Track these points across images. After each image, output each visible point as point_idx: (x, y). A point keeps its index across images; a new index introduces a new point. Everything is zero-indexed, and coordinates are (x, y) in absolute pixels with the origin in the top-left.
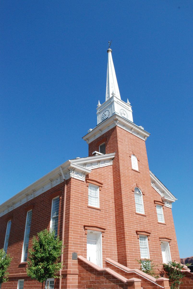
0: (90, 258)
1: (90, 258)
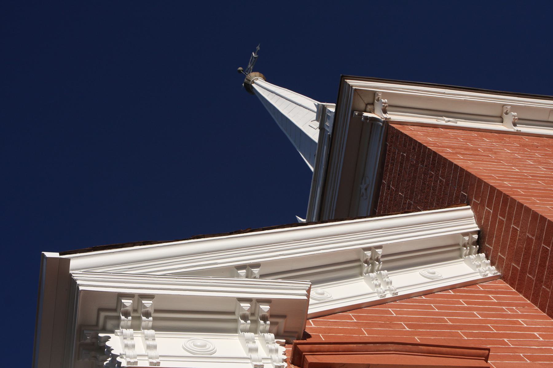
0: (309, 126)
1: (309, 126)
